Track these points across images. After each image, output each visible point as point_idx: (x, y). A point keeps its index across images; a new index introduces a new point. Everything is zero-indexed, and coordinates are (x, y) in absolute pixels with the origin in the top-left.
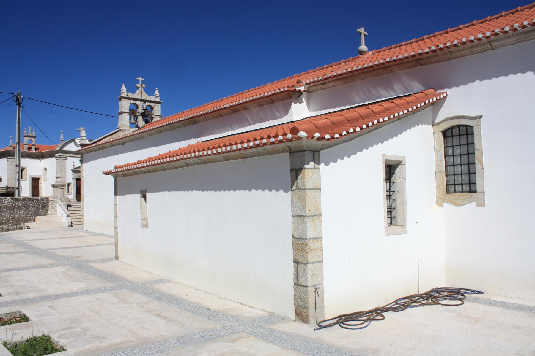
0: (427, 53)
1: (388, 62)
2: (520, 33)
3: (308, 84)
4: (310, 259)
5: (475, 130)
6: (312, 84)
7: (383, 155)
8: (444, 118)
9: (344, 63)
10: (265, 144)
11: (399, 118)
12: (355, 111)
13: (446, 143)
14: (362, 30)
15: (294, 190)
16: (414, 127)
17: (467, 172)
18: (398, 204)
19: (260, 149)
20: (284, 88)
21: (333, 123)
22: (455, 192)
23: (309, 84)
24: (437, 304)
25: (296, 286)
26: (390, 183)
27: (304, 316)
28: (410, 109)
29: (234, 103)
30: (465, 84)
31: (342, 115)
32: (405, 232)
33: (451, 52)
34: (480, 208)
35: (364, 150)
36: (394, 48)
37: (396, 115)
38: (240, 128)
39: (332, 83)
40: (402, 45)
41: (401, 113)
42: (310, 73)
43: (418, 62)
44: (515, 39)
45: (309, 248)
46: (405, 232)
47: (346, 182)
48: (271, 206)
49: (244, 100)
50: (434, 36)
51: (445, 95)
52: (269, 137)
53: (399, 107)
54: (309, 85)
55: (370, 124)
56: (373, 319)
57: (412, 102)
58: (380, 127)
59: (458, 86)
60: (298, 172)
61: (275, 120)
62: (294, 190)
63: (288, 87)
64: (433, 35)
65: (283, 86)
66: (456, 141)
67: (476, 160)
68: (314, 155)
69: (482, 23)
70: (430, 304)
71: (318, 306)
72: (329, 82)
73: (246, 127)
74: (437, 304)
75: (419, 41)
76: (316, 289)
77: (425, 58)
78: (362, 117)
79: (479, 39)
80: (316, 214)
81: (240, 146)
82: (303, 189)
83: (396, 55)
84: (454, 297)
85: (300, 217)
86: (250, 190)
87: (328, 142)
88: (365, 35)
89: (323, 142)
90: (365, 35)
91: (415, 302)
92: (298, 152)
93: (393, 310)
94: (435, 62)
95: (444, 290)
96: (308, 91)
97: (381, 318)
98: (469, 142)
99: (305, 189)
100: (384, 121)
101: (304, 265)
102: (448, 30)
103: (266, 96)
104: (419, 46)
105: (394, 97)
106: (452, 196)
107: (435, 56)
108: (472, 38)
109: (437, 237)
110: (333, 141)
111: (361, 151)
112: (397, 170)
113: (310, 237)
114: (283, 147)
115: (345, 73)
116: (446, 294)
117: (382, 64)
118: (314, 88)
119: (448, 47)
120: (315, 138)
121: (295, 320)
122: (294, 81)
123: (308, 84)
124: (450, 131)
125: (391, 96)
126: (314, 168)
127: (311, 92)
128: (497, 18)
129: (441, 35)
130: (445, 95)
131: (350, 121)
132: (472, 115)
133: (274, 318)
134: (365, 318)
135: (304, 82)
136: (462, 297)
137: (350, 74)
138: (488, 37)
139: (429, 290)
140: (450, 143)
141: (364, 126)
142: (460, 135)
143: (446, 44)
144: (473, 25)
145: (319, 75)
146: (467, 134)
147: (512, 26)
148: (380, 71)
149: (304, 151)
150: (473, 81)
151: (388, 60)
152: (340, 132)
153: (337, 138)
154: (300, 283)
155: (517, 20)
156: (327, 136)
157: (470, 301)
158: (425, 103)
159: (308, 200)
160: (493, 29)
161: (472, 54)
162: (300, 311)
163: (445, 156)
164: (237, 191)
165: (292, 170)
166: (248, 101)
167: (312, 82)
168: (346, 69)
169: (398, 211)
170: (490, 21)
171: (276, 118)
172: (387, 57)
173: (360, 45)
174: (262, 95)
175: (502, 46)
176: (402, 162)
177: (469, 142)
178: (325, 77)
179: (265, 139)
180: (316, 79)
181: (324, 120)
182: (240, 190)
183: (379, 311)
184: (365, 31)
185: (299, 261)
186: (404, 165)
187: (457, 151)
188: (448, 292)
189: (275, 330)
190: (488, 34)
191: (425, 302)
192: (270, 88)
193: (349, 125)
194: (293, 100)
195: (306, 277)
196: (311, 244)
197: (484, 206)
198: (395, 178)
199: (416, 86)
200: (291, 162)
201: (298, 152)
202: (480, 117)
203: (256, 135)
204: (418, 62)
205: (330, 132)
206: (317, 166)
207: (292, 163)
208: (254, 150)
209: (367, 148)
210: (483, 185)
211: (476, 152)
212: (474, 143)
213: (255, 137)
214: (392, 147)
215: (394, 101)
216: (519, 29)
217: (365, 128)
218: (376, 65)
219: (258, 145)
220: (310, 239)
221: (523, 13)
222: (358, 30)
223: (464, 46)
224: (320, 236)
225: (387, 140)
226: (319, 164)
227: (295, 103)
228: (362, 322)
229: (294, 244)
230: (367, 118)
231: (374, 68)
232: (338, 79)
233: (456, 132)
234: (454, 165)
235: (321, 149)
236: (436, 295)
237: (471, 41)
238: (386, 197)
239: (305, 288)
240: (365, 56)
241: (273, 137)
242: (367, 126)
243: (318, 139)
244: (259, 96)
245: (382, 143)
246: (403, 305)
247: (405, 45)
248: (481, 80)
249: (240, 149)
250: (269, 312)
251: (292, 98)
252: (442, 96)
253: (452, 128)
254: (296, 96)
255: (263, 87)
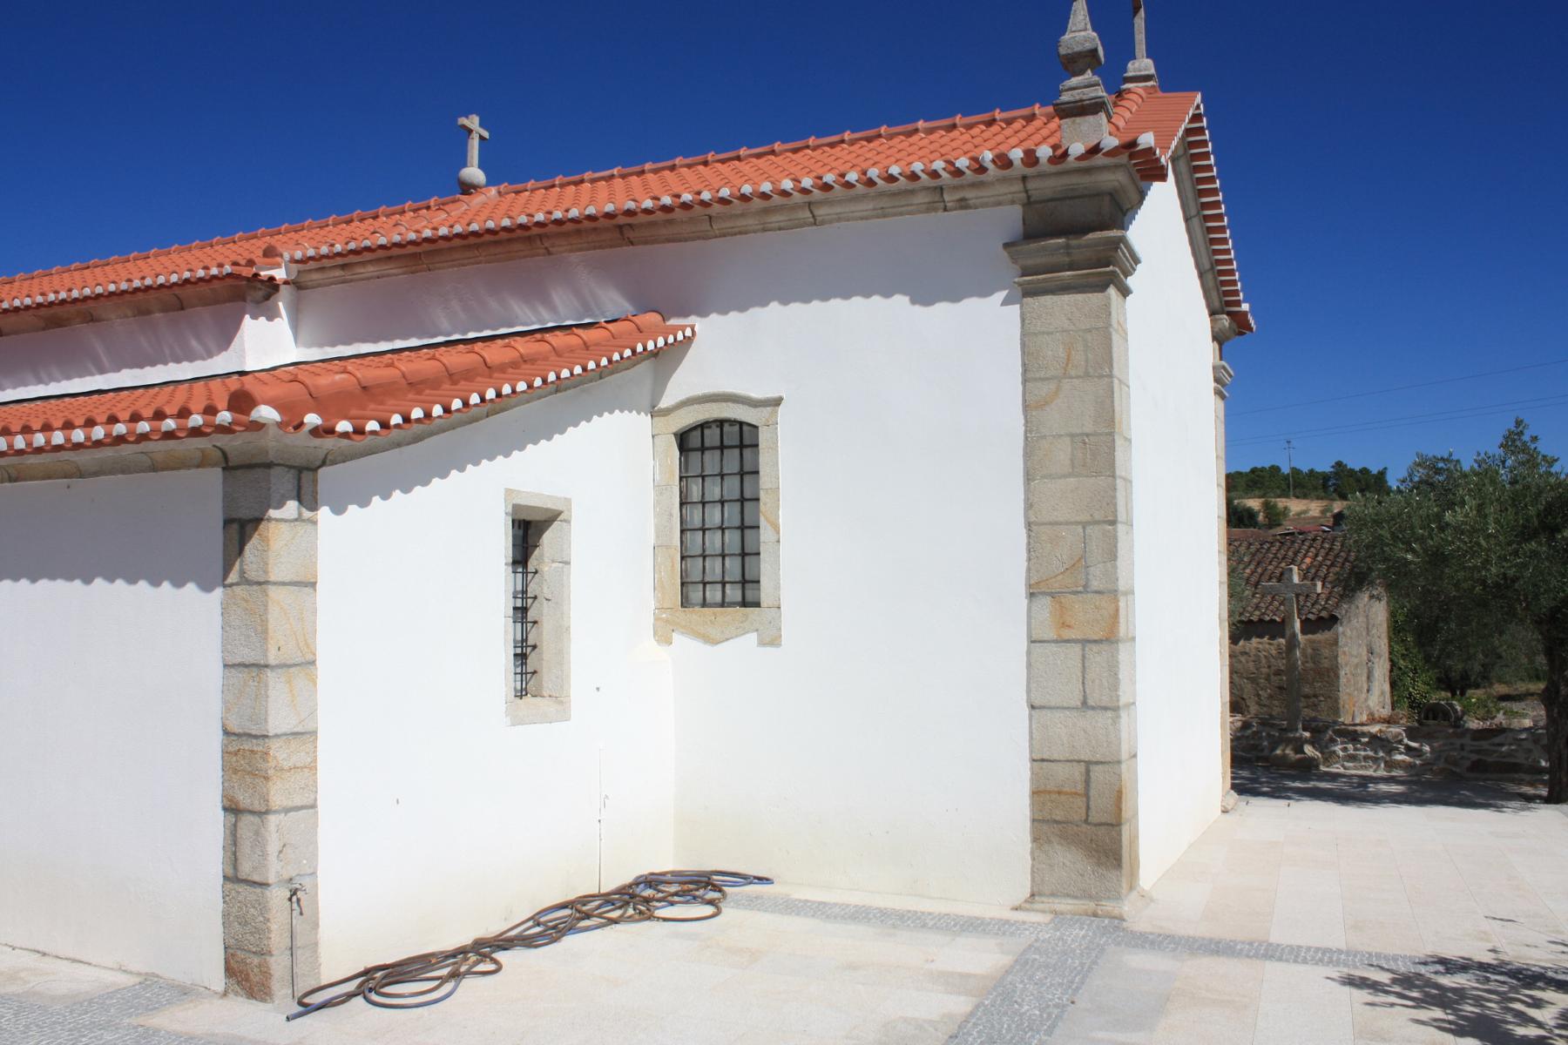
0: (647, 211)
1: (538, 224)
2: (882, 194)
3: (297, 262)
4: (277, 798)
5: (764, 437)
6: (312, 265)
7: (509, 492)
8: (682, 397)
9: (415, 211)
10: (144, 437)
11: (560, 386)
12: (433, 358)
13: (684, 466)
14: (473, 122)
15: (231, 585)
16: (600, 415)
17: (738, 551)
18: (544, 635)
19: (126, 450)
20: (220, 266)
21: (364, 388)
22: (704, 604)
23: (305, 260)
24: (651, 917)
25: (229, 886)
26: (525, 573)
27: (255, 978)
28: (591, 365)
29: (52, 297)
30: (742, 308)
31: (391, 365)
32: (564, 716)
33: (941, 189)
34: (769, 649)
35: (454, 473)
36: (562, 186)
37: (552, 377)
38: (69, 378)
39: (371, 268)
40: (582, 181)
41: (565, 373)
42: (310, 228)
43: (622, 233)
44: (871, 206)
45: (272, 764)
46: (564, 716)
47: (390, 567)
48: (162, 630)
49: (87, 291)
50: (673, 168)
51: (688, 333)
52: (159, 415)
53: (561, 356)
54: (300, 266)
55: (474, 399)
56: (469, 972)
57: (597, 344)
58: (502, 410)
59: (724, 312)
60: (249, 528)
61: (185, 364)
62: (231, 585)
63: (235, 264)
64: (669, 163)
65: (220, 259)
66: (712, 461)
67: (762, 519)
68: (299, 480)
69: (795, 151)
70: (630, 919)
71: (299, 942)
72: (363, 264)
73: (88, 378)
74: (649, 918)
75: (631, 174)
76: (294, 892)
77: (641, 225)
78: (453, 377)
79: (785, 193)
80: (298, 660)
81: (58, 438)
82: (259, 583)
83: (565, 207)
84: (695, 898)
85: (247, 670)
86: (88, 580)
87: (345, 442)
88: (481, 138)
89: (329, 443)
90: (481, 138)
91: (588, 916)
92: (250, 466)
93: (527, 942)
94: (669, 241)
95: (669, 877)
96: (297, 284)
97: (492, 967)
98: (746, 469)
99: (267, 582)
100: (514, 391)
101: (256, 819)
102: (710, 157)
103: (162, 286)
104: (628, 189)
105: (550, 325)
106: (697, 615)
107: (670, 222)
108: (766, 187)
109: (652, 730)
110: (360, 443)
111: (444, 475)
112: (548, 537)
113: (279, 732)
114: (202, 451)
115: (412, 243)
116: (673, 889)
117: (521, 226)
118: (316, 276)
119: (703, 203)
120: (306, 429)
121: (225, 994)
122: (254, 248)
123: (297, 262)
124: (698, 433)
125: (540, 322)
126: (299, 519)
127: (306, 288)
128: (832, 145)
129: (689, 166)
130: (688, 333)
131: (417, 386)
132: (756, 394)
133: (156, 991)
134: (445, 972)
135: (287, 256)
136: (716, 895)
137: (426, 247)
138: (805, 191)
139: (626, 878)
140: (695, 469)
141: (457, 404)
142: (722, 448)
143: (699, 193)
144: (773, 152)
145: (336, 237)
146: (742, 446)
147: (865, 173)
148: (517, 246)
149: (269, 465)
150: (764, 304)
151: (540, 217)
152: (384, 415)
153: (373, 433)
154: (242, 875)
155: (876, 159)
156: (344, 426)
157: (738, 905)
158: (634, 352)
159: (274, 615)
160: (820, 172)
161: (764, 230)
162: (243, 961)
163: (682, 504)
164: (44, 584)
165: (227, 522)
166: (99, 296)
167: (311, 258)
168: (417, 231)
169: (546, 656)
170: (815, 149)
171: (191, 357)
172: (538, 210)
173: (465, 165)
174: (148, 282)
175: (839, 220)
176: (560, 513)
177: (746, 469)
178: (352, 246)
179: (147, 420)
180: (324, 250)
181: (338, 377)
182: (53, 577)
183: (486, 949)
184: (481, 125)
185: (242, 806)
186: (568, 521)
187: (714, 491)
188: (681, 883)
189: (156, 1031)
190: (807, 182)
191: (615, 914)
192: (180, 261)
193: (411, 396)
194: (249, 306)
195: (264, 855)
196: (280, 753)
197: (779, 645)
198: (541, 560)
199: (613, 302)
200: (226, 495)
201: (250, 466)
202: (777, 402)
203: (142, 402)
204: (622, 233)
205: (354, 412)
206: (307, 514)
207: (229, 500)
208: (108, 452)
209: (462, 469)
210: (777, 587)
211: (762, 495)
212: (757, 472)
213: (115, 410)
214: (535, 470)
215: (547, 336)
216: (944, 175)
217: (458, 410)
218: (505, 229)
219: (120, 439)
220: (277, 736)
221: (891, 143)
222: (463, 121)
223: (745, 205)
224: (309, 728)
225: (522, 448)
226: (314, 507)
227: (254, 317)
228: (437, 983)
229: (225, 752)
230: (466, 379)
231: (496, 238)
232: (390, 258)
233: (712, 436)
234: (704, 530)
235: (324, 464)
236: (649, 892)
237: (765, 196)
238: (511, 612)
239: (258, 890)
240: (477, 200)
241: (171, 416)
242: (466, 404)
243: (316, 432)
244: (137, 283)
245: (507, 455)
246: (554, 927)
247: (593, 181)
248: (785, 301)
249: (59, 448)
250: (139, 974)
251: (244, 300)
252: (680, 337)
253: (703, 426)
254: (260, 294)
255: (135, 259)
